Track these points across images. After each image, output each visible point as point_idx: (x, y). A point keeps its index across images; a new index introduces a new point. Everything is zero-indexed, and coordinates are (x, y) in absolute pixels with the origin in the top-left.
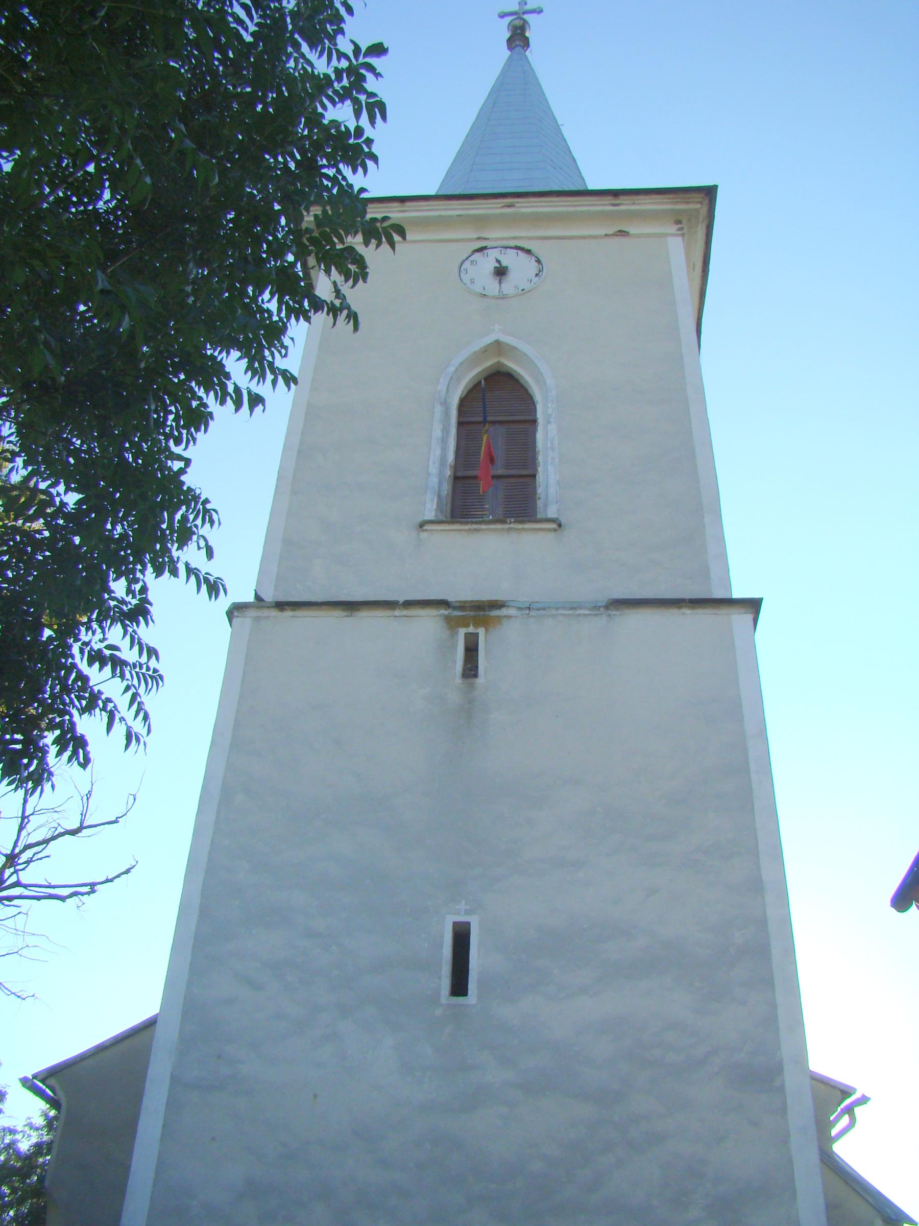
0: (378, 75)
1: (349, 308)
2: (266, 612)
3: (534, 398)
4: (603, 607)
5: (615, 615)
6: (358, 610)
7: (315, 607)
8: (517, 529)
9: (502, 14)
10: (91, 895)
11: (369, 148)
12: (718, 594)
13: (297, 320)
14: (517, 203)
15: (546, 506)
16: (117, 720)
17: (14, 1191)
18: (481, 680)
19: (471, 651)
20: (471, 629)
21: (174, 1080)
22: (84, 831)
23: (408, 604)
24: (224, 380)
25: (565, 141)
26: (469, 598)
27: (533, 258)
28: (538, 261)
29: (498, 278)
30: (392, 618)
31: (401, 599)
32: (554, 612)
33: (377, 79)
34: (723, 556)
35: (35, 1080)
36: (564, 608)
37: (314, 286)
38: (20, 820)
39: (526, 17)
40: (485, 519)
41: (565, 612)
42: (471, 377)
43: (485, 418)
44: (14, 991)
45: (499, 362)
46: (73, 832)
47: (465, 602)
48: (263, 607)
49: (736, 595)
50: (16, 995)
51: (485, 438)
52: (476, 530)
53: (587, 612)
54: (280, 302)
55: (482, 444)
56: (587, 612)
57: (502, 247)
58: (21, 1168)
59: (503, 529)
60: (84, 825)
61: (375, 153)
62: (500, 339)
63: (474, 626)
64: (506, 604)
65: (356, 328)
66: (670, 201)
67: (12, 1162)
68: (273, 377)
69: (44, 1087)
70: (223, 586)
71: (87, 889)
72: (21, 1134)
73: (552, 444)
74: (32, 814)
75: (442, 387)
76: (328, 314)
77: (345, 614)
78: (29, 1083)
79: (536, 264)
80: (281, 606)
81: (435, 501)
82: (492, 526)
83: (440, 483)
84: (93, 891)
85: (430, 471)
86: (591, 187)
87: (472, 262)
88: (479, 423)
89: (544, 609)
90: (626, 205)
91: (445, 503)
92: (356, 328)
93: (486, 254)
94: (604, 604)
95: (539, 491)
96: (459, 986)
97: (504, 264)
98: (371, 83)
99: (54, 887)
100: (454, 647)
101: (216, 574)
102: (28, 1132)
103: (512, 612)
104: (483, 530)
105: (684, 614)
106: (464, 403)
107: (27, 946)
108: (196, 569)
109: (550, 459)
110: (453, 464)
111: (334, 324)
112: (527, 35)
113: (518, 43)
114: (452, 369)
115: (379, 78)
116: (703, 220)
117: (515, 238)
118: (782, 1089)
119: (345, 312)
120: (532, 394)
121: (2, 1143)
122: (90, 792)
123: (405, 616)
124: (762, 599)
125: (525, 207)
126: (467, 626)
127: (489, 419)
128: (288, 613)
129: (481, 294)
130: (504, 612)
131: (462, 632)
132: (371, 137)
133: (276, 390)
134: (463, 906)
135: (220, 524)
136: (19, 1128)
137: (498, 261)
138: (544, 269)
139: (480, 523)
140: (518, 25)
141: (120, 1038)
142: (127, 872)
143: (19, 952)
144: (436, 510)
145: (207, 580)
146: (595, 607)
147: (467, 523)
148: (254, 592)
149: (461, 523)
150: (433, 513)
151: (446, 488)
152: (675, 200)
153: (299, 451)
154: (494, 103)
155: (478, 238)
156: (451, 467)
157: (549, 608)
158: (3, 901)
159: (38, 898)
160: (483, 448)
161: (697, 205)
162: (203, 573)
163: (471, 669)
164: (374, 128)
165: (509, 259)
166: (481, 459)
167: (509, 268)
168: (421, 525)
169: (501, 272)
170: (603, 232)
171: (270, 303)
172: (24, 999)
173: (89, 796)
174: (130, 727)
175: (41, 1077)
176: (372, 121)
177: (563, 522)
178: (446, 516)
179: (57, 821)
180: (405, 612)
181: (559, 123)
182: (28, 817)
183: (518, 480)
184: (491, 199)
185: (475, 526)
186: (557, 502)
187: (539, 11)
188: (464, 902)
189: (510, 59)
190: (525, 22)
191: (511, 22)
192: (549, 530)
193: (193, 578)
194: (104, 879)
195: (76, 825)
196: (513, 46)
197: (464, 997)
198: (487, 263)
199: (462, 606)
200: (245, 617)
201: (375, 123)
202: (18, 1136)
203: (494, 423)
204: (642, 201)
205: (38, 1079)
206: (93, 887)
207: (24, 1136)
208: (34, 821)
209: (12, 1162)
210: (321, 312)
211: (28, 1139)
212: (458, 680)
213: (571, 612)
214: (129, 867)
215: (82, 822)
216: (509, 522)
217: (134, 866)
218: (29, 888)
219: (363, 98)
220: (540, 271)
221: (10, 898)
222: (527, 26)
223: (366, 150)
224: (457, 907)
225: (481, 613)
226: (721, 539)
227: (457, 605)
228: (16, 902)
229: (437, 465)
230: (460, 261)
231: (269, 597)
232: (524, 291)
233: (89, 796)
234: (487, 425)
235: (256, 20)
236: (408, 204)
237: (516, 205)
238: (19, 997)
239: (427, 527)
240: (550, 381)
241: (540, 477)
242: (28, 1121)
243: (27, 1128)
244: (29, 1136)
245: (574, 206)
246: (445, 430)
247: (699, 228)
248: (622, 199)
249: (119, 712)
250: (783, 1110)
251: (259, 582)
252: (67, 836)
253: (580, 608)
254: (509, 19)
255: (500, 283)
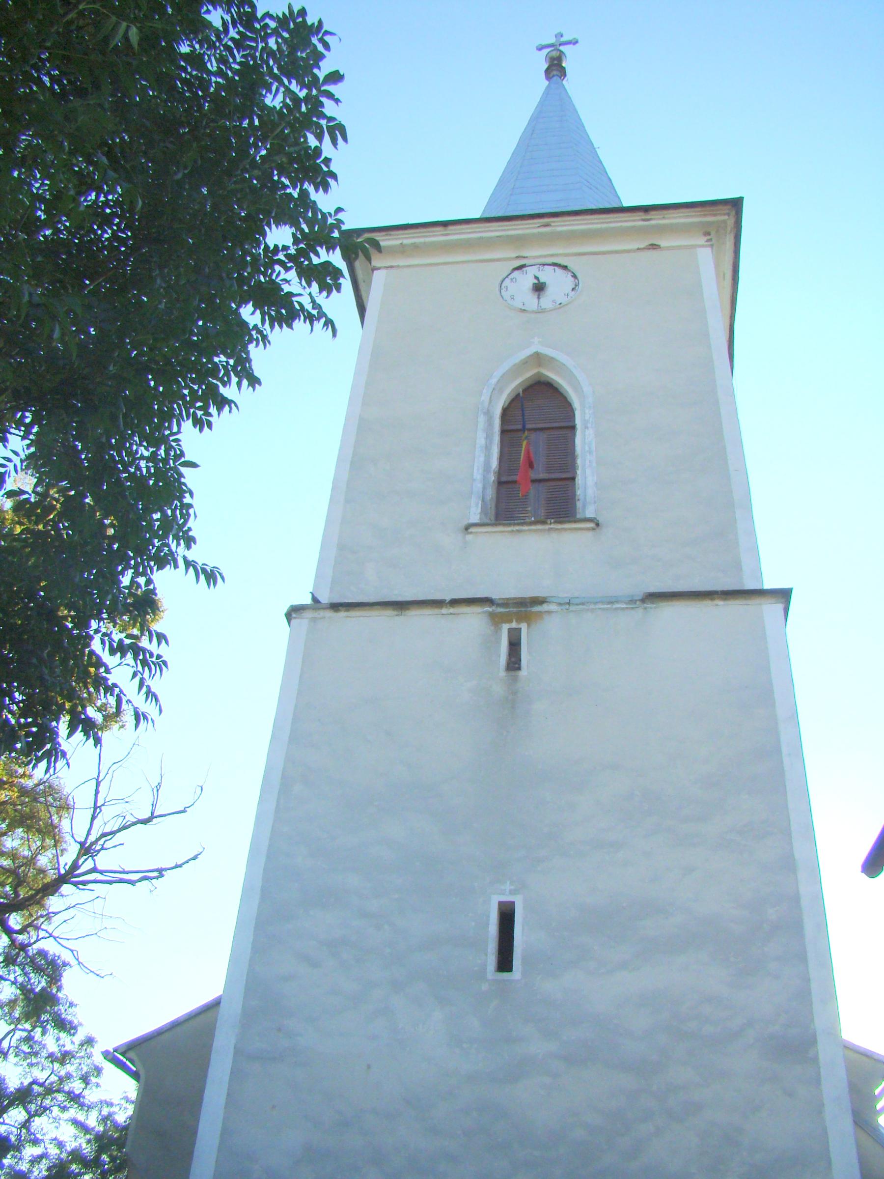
0: (337, 101)
1: (325, 315)
2: (322, 613)
3: (572, 405)
4: (639, 600)
5: (651, 608)
6: (408, 609)
7: (368, 608)
8: (557, 529)
9: (540, 47)
10: (159, 879)
11: (328, 167)
12: (750, 585)
13: (281, 327)
14: (554, 222)
15: (584, 506)
16: (124, 702)
17: (113, 1159)
18: (523, 673)
19: (514, 646)
20: (514, 625)
21: (238, 1052)
22: (155, 820)
23: (454, 602)
24: (191, 385)
25: (601, 162)
26: (513, 596)
27: (569, 273)
28: (575, 276)
29: (537, 293)
30: (439, 616)
31: (448, 598)
32: (592, 606)
33: (338, 105)
34: (754, 549)
35: (115, 1053)
36: (602, 603)
37: (365, 306)
38: (92, 809)
39: (562, 48)
40: (528, 520)
41: (602, 606)
42: (513, 387)
43: (524, 426)
44: (92, 970)
45: (539, 373)
46: (145, 822)
47: (508, 599)
48: (319, 609)
49: (767, 586)
50: (95, 974)
51: (525, 443)
52: (519, 531)
53: (624, 606)
54: (263, 314)
55: (521, 450)
56: (624, 606)
57: (540, 265)
58: (119, 1138)
59: (541, 530)
60: (155, 815)
61: (334, 171)
62: (539, 351)
63: (516, 621)
64: (548, 600)
65: (334, 334)
66: (699, 214)
67: (111, 1133)
68: (237, 379)
69: (125, 1060)
70: (220, 574)
71: (156, 874)
72: (118, 1107)
73: (590, 448)
74: (103, 805)
75: (485, 398)
76: (305, 322)
77: (395, 613)
78: (110, 1056)
79: (572, 279)
80: (335, 607)
81: (480, 506)
82: (533, 527)
83: (484, 488)
84: (162, 876)
85: (475, 477)
86: (626, 204)
87: (512, 280)
88: (517, 430)
89: (583, 604)
90: (657, 220)
91: (489, 507)
92: (334, 334)
93: (525, 272)
94: (640, 598)
95: (579, 492)
96: (505, 962)
97: (542, 280)
98: (329, 107)
99: (127, 872)
100: (498, 641)
101: (212, 565)
102: (124, 1105)
103: (553, 607)
104: (525, 531)
105: (717, 605)
106: (505, 412)
107: (106, 928)
108: (193, 561)
109: (587, 462)
110: (497, 470)
111: (312, 330)
112: (564, 65)
113: (555, 73)
114: (494, 381)
115: (339, 104)
116: (731, 230)
117: (552, 255)
118: (815, 1059)
119: (323, 320)
120: (571, 402)
121: (100, 1114)
122: (160, 784)
123: (451, 614)
124: (792, 589)
125: (561, 226)
126: (510, 621)
127: (528, 426)
128: (342, 614)
129: (521, 309)
130: (545, 607)
131: (505, 627)
132: (329, 157)
133: (241, 392)
134: (507, 886)
135: (196, 516)
136: (115, 1102)
137: (536, 278)
138: (580, 285)
139: (522, 524)
140: (555, 57)
141: (193, 1014)
142: (195, 858)
143: (98, 934)
144: (481, 513)
145: (204, 571)
146: (631, 601)
147: (510, 525)
148: (311, 595)
149: (504, 525)
150: (478, 517)
151: (491, 493)
152: (702, 213)
153: (352, 462)
154: (533, 130)
155: (517, 257)
156: (495, 473)
157: (588, 603)
158: (79, 885)
159: (110, 882)
160: (522, 454)
161: (725, 217)
162: (200, 564)
163: (514, 663)
164: (336, 148)
165: (547, 275)
166: (521, 462)
167: (547, 284)
168: (467, 528)
169: (539, 288)
170: (636, 246)
171: (249, 314)
172: (103, 977)
173: (158, 787)
174: (137, 708)
175: (120, 1051)
176: (334, 142)
177: (601, 520)
178: (490, 519)
179: (130, 812)
180: (452, 610)
181: (595, 146)
182: (100, 807)
183: (560, 483)
184: (528, 219)
185: (517, 528)
186: (595, 502)
187: (575, 42)
188: (508, 882)
189: (548, 88)
190: (561, 52)
191: (548, 53)
192: (588, 529)
193: (191, 570)
194: (173, 865)
195: (147, 815)
196: (551, 75)
197: (509, 973)
198: (526, 280)
199: (506, 603)
200: (301, 618)
201: (337, 144)
202: (115, 1109)
203: (529, 430)
204: (671, 216)
205: (119, 1052)
206: (161, 872)
207: (121, 1109)
208: (107, 813)
209: (111, 1133)
210: (297, 320)
211: (125, 1111)
212: (502, 673)
213: (609, 606)
214: (197, 853)
215: (153, 813)
216: (549, 522)
217: (202, 852)
218: (104, 874)
219: (323, 122)
220: (576, 286)
221: (84, 883)
222: (563, 58)
223: (325, 169)
224: (503, 887)
225: (523, 609)
226: (752, 533)
227: (500, 602)
228: (90, 886)
229: (481, 471)
230: (501, 279)
231: (325, 599)
232: (561, 305)
233: (158, 787)
234: (526, 432)
235: (238, 60)
236: (451, 228)
237: (552, 224)
238: (98, 975)
239: (472, 530)
240: (587, 389)
241: (579, 480)
242: (124, 1095)
243: (123, 1102)
244: (126, 1108)
245: (607, 223)
246: (489, 438)
247: (727, 239)
248: (653, 214)
249: (125, 695)
250: (818, 1082)
251: (316, 585)
252: (139, 825)
253: (617, 602)
254: (546, 51)
255: (539, 298)
